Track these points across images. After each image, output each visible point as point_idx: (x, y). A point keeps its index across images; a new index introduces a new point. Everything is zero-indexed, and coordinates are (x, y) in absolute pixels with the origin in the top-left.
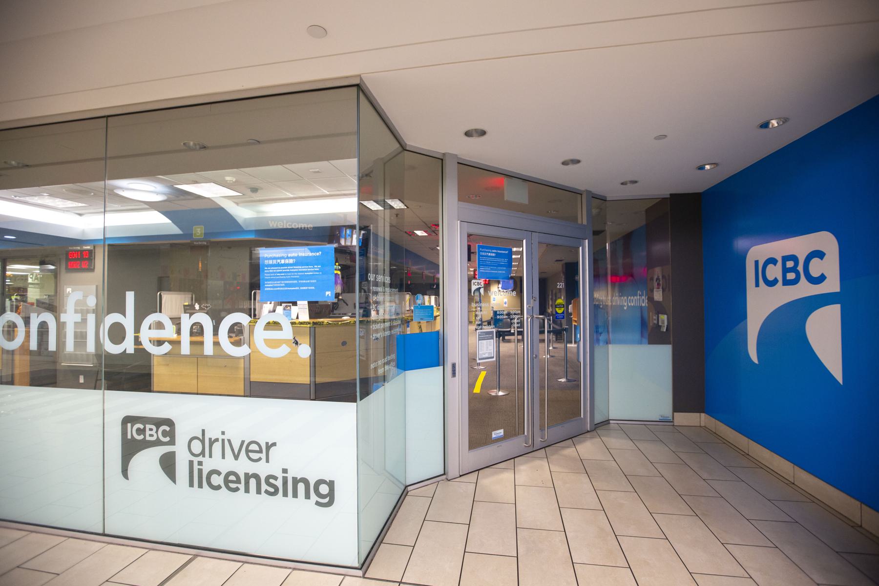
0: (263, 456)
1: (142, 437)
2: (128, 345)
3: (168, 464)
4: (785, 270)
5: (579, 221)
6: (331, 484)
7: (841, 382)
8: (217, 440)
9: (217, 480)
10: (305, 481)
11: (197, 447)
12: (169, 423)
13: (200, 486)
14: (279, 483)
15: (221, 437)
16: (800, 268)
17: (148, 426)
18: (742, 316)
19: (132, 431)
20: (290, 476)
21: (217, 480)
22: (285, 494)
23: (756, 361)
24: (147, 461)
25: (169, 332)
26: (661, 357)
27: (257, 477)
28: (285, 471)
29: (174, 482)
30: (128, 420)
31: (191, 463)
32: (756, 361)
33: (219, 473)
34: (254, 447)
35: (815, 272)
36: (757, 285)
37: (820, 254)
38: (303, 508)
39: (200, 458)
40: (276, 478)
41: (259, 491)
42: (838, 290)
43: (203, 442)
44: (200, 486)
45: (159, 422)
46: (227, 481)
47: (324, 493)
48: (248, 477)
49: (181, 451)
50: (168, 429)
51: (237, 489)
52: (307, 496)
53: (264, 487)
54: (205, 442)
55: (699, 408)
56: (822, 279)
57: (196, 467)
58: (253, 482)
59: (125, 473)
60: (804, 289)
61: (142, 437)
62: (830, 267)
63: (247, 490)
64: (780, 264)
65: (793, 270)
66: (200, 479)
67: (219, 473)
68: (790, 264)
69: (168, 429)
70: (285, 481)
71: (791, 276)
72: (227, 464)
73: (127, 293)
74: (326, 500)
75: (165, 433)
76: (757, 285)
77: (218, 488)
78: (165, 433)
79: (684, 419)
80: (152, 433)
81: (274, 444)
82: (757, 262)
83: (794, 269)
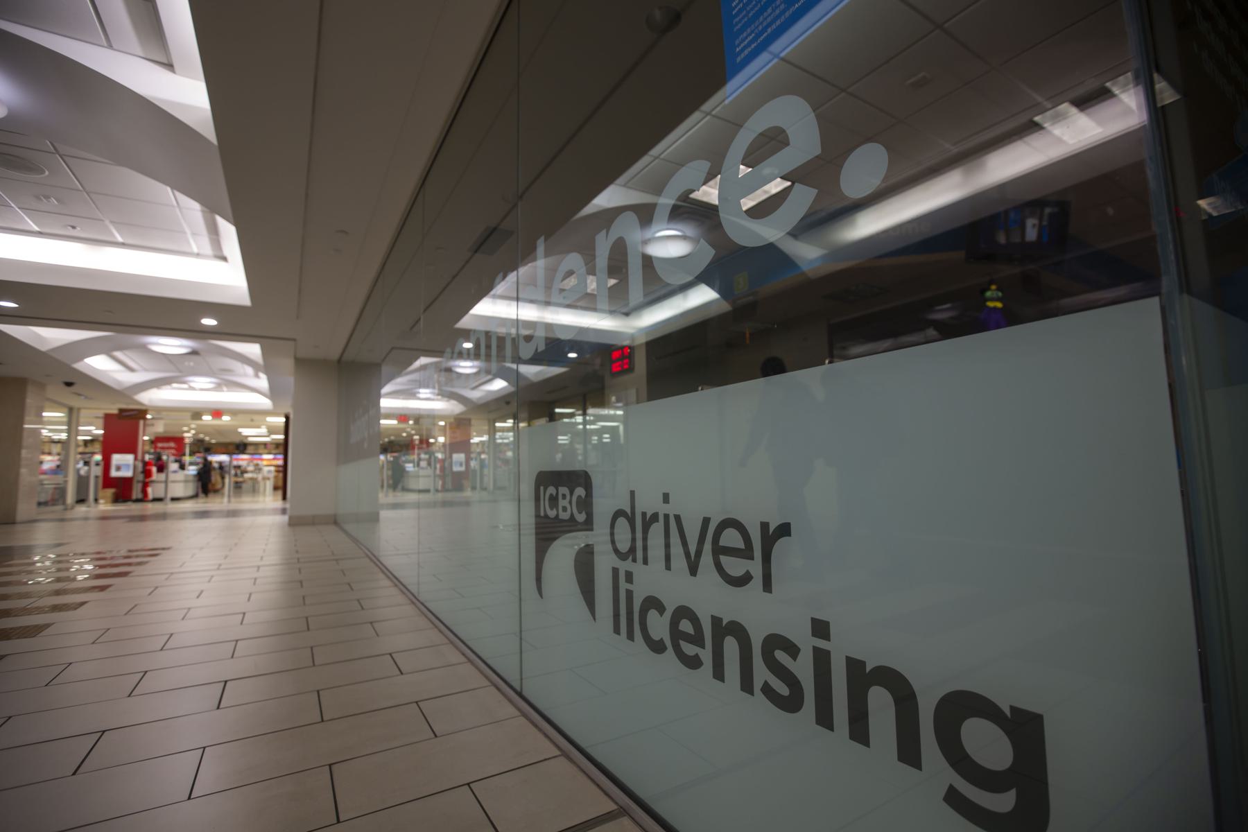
0: (755, 567)
8: (655, 517)
14: (761, 673)
15: (662, 509)
27: (737, 630)
28: (821, 629)
31: (615, 571)
43: (631, 521)
48: (723, 629)
70: (822, 660)
81: (784, 530)
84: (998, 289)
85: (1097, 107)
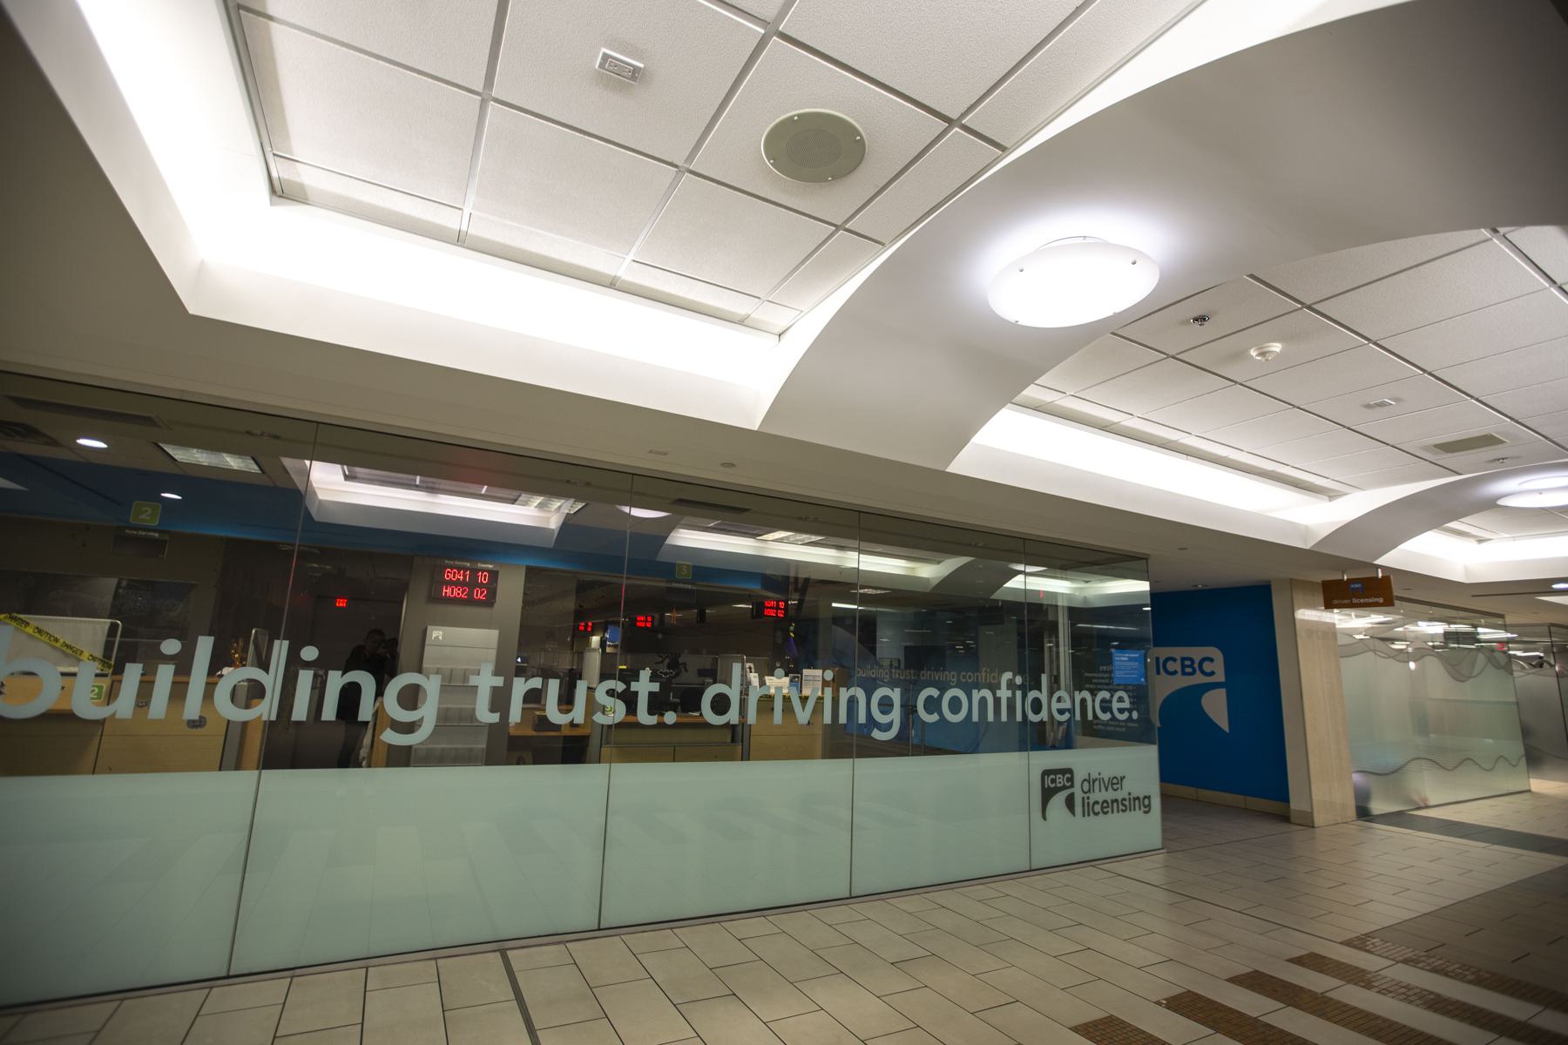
3: (1070, 803)
4: (1183, 666)
9: (1097, 808)
12: (1070, 771)
23: (1223, 722)
24: (1058, 800)
25: (1067, 705)
30: (1046, 773)
37: (1211, 660)
38: (1138, 814)
42: (141, 666)
47: (1143, 803)
49: (1077, 790)
56: (1212, 673)
59: (1044, 817)
60: (1199, 679)
65: (1188, 666)
66: (1089, 809)
71: (1188, 670)
73: (331, 673)
83: (1191, 666)
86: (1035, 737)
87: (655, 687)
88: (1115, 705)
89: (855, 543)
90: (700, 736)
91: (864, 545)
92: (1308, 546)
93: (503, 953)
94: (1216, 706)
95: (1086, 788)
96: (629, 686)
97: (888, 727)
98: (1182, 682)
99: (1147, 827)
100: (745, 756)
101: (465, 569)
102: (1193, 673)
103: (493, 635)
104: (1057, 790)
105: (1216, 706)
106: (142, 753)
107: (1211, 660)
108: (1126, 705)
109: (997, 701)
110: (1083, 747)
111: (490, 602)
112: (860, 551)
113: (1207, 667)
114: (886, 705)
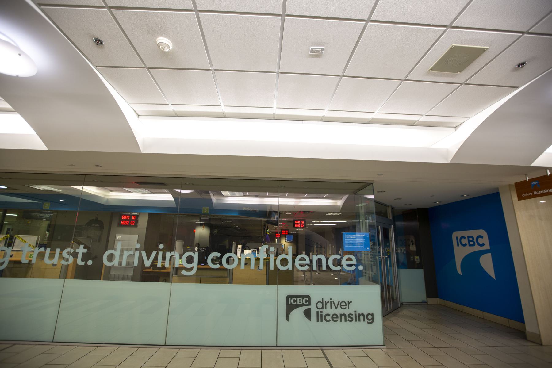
0: (347, 307)
1: (296, 303)
2: (289, 267)
3: (307, 314)
4: (469, 241)
5: (389, 218)
6: (372, 315)
7: (494, 278)
8: (328, 302)
10: (363, 315)
11: (320, 305)
12: (308, 297)
13: (322, 321)
14: (348, 318)
15: (330, 301)
16: (475, 241)
17: (298, 299)
18: (453, 256)
19: (291, 301)
20: (357, 313)
21: (328, 318)
22: (356, 321)
23: (461, 274)
24: (298, 314)
26: (418, 274)
27: (345, 315)
28: (355, 312)
29: (310, 320)
30: (289, 297)
31: (318, 312)
32: (461, 274)
33: (329, 315)
34: (343, 304)
35: (481, 243)
36: (458, 245)
37: (482, 237)
38: (362, 325)
39: (321, 310)
40: (352, 315)
41: (346, 321)
43: (322, 303)
44: (322, 321)
45: (303, 297)
46: (332, 318)
47: (369, 318)
48: (341, 315)
50: (307, 299)
51: (337, 321)
52: (364, 320)
53: (348, 318)
54: (324, 303)
55: (436, 296)
56: (483, 245)
57: (320, 313)
58: (343, 317)
60: (477, 248)
61: (296, 303)
62: (485, 240)
63: (341, 321)
64: (467, 238)
65: (472, 241)
66: (321, 318)
67: (329, 315)
68: (471, 239)
69: (307, 299)
70: (355, 315)
71: (472, 243)
72: (333, 311)
74: (371, 321)
75: (306, 301)
76: (458, 245)
77: (329, 321)
78: (306, 301)
79: (432, 301)
80: (300, 301)
81: (351, 302)
82: (457, 238)
83: (472, 241)
84: (84, 248)
85: (282, 115)
86: (275, 277)
87: (85, 251)
88: (344, 262)
89: (277, 194)
90: (208, 273)
91: (281, 194)
92: (448, 161)
93: (322, 350)
94: (487, 263)
95: (320, 305)
96: (75, 250)
97: (191, 269)
98: (469, 250)
99: (375, 332)
100: (231, 282)
101: (128, 215)
102: (474, 245)
103: (136, 237)
104: (297, 306)
105: (487, 263)
106: (42, 275)
107: (482, 237)
108: (354, 261)
109: (257, 260)
110: (365, 284)
111: (136, 225)
112: (279, 197)
113: (480, 241)
114: (190, 260)
